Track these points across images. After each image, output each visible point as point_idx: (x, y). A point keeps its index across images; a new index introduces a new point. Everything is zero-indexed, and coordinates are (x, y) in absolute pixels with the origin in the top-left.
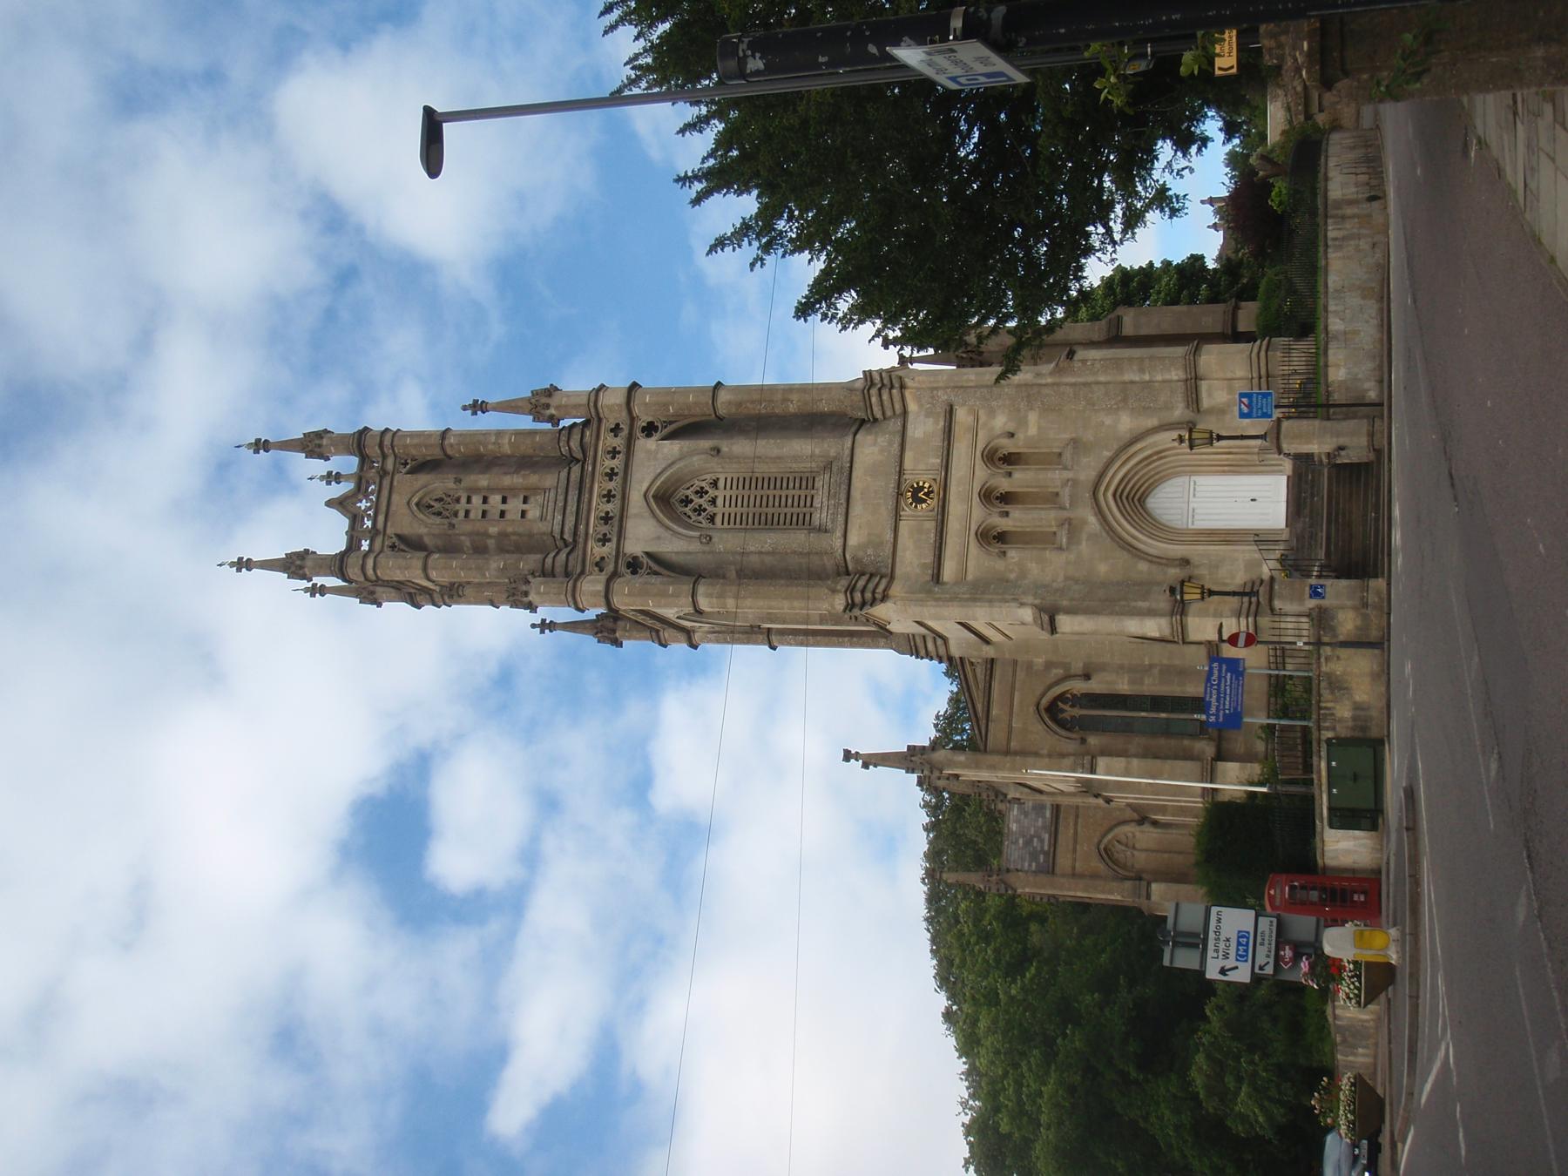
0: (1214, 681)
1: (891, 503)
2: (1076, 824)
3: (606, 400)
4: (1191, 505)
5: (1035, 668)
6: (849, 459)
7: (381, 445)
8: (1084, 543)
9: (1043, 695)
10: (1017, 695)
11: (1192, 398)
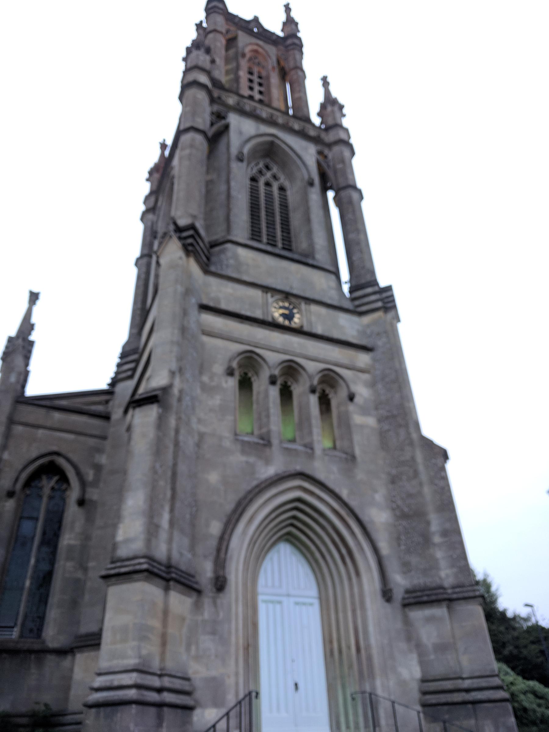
4: (284, 600)
8: (243, 458)
9: (68, 460)
10: (71, 437)
11: (421, 596)
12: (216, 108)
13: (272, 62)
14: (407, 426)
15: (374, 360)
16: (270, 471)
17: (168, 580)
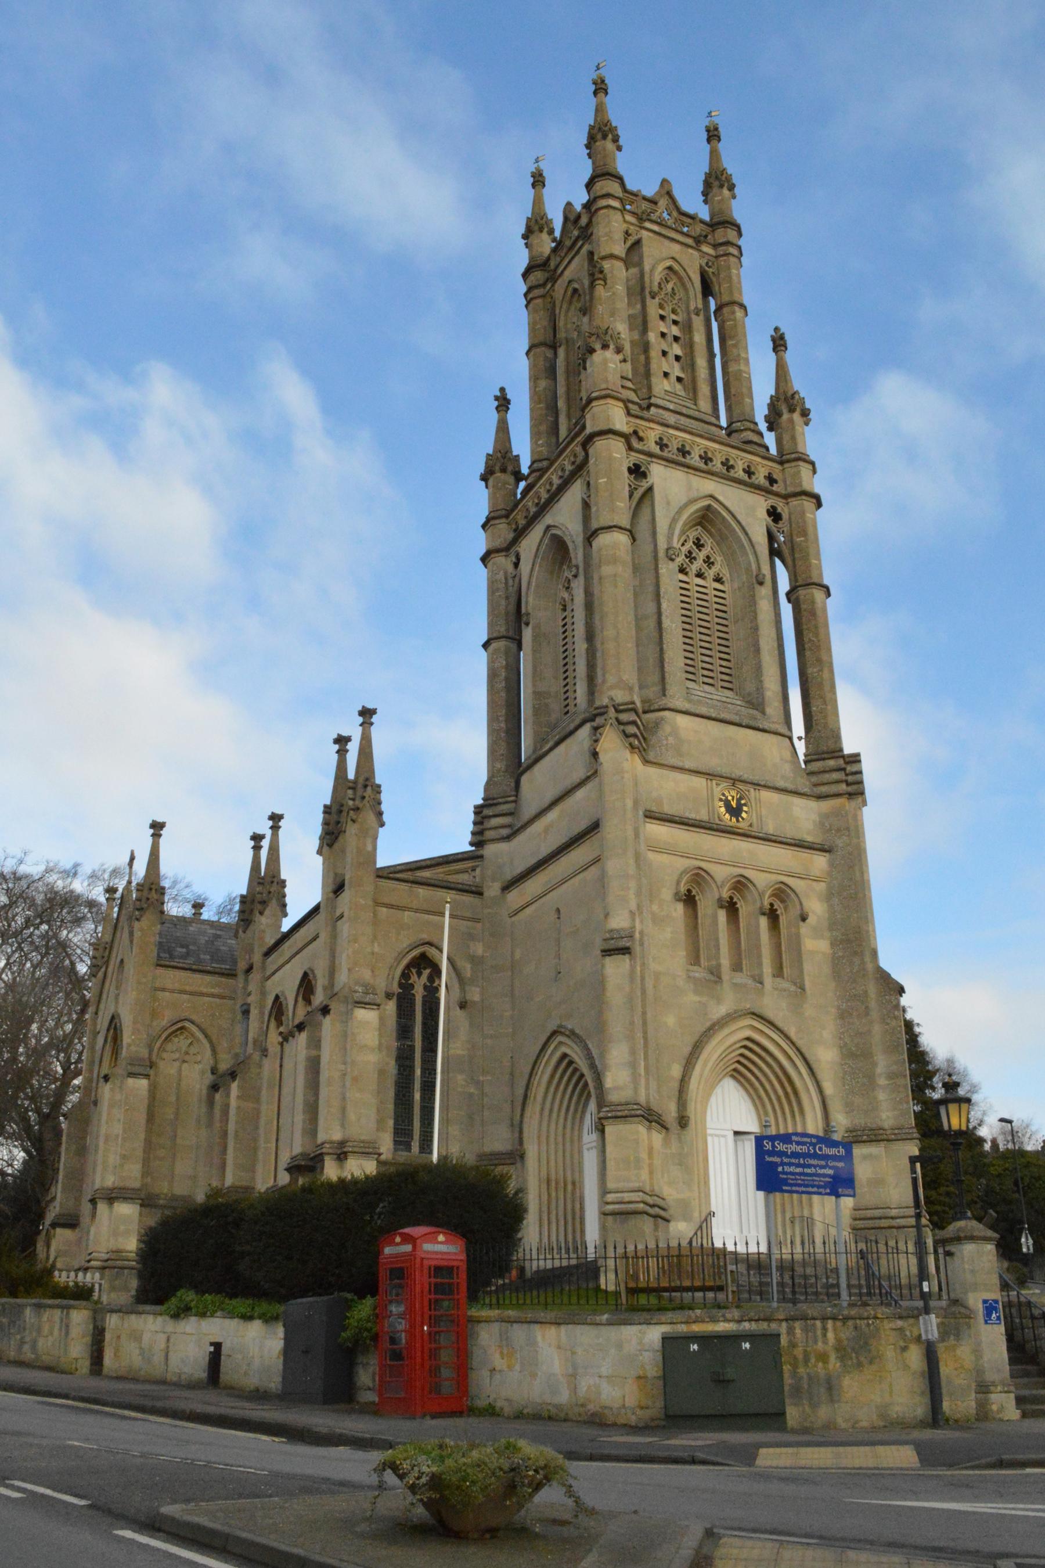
0: (820, 1149)
1: (725, 771)
2: (213, 996)
3: (805, 469)
5: (471, 944)
6: (766, 727)
7: (728, 243)
8: (696, 998)
12: (635, 458)
13: (758, 527)
14: (862, 954)
15: (831, 864)
16: (720, 1010)
17: (650, 1122)
